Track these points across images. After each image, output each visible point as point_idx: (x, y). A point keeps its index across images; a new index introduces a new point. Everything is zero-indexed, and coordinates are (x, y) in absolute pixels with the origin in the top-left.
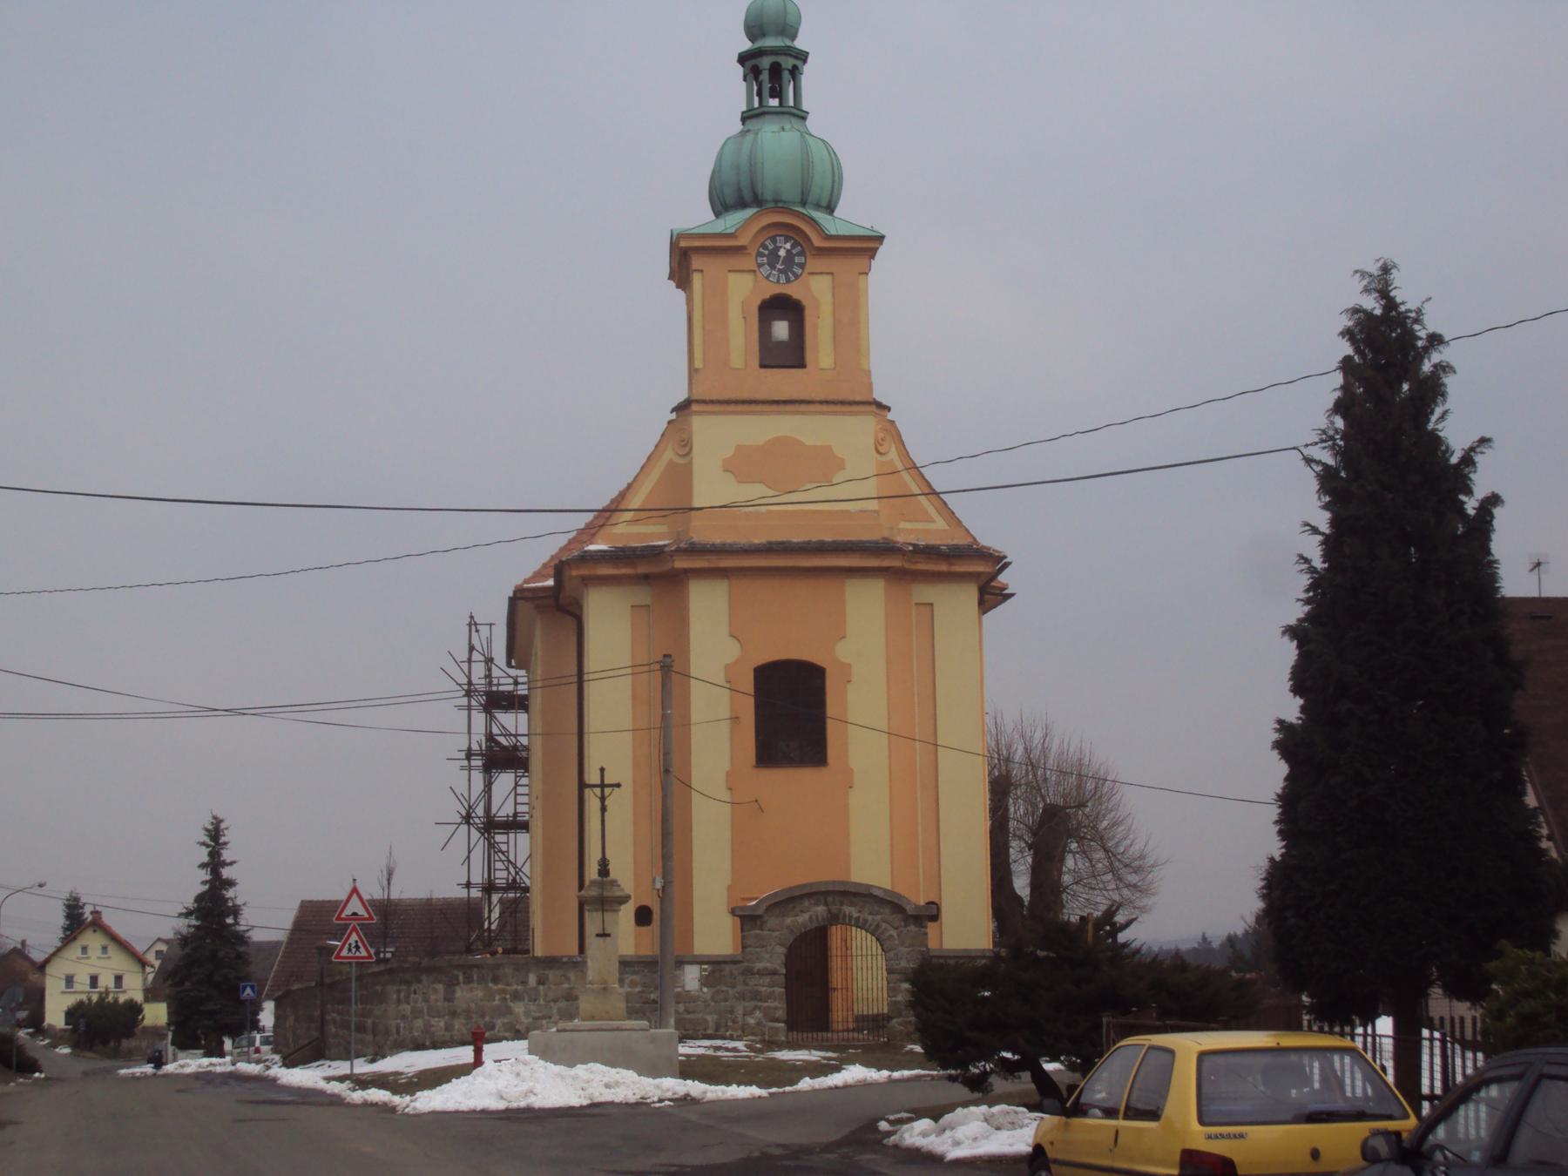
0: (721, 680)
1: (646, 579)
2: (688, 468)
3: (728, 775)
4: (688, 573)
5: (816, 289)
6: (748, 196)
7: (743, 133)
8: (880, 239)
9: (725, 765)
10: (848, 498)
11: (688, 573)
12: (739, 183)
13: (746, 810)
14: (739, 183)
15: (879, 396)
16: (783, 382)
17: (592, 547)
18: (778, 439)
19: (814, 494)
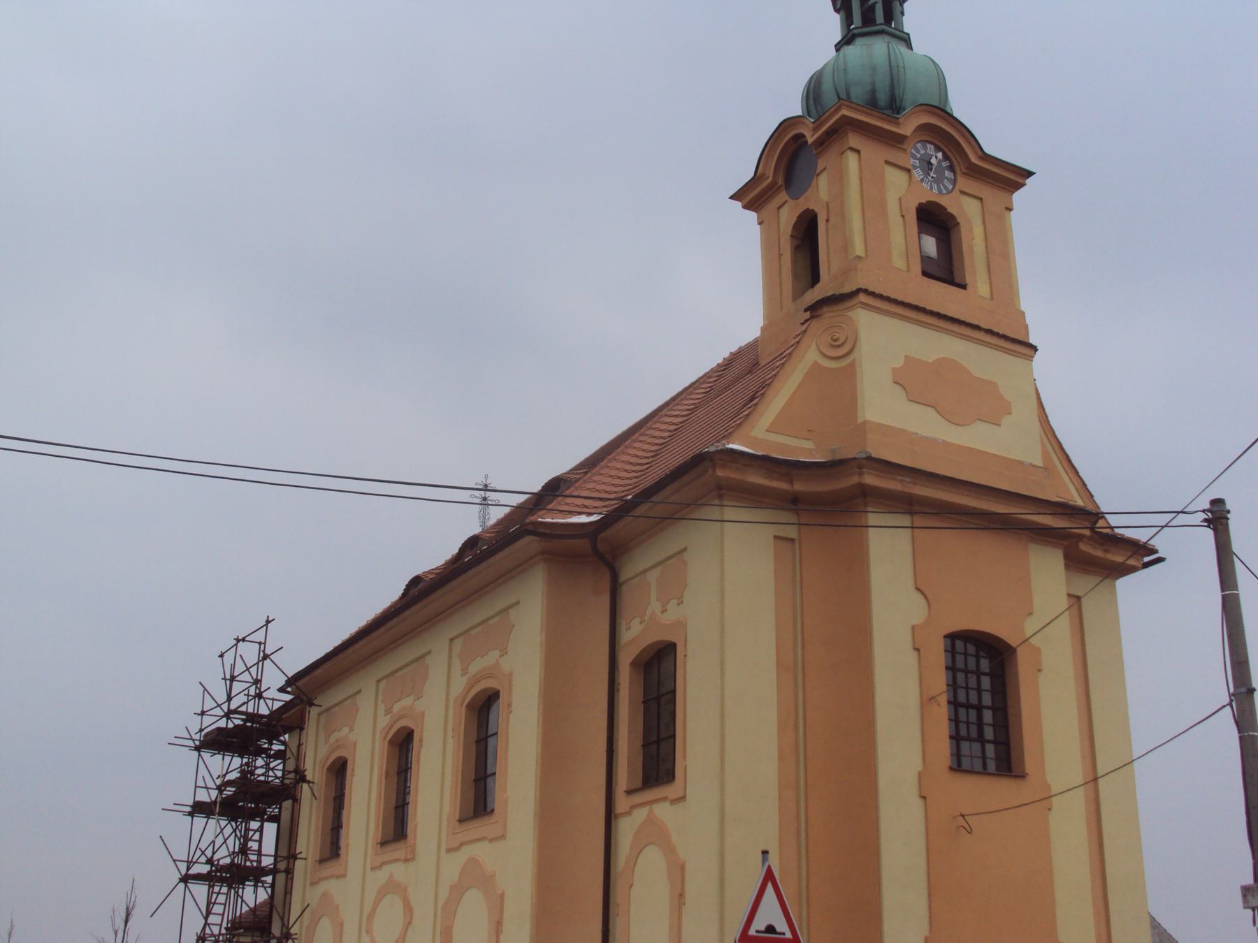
0: (1033, 641)
1: (794, 502)
2: (850, 373)
3: (920, 774)
4: (866, 495)
5: (967, 209)
6: (882, 98)
7: (837, 56)
8: (1030, 174)
9: (916, 764)
10: (991, 446)
11: (866, 495)
12: (873, 84)
13: (946, 834)
14: (873, 84)
15: (1032, 341)
16: (938, 296)
17: (731, 446)
18: (943, 359)
19: (978, 437)
